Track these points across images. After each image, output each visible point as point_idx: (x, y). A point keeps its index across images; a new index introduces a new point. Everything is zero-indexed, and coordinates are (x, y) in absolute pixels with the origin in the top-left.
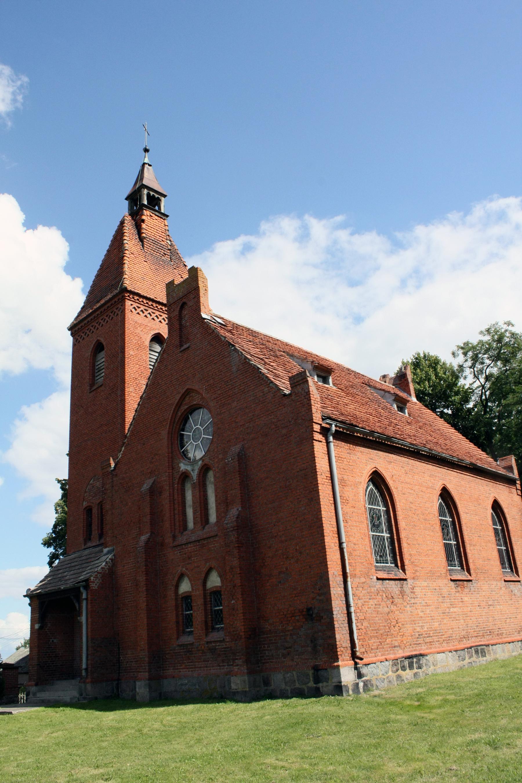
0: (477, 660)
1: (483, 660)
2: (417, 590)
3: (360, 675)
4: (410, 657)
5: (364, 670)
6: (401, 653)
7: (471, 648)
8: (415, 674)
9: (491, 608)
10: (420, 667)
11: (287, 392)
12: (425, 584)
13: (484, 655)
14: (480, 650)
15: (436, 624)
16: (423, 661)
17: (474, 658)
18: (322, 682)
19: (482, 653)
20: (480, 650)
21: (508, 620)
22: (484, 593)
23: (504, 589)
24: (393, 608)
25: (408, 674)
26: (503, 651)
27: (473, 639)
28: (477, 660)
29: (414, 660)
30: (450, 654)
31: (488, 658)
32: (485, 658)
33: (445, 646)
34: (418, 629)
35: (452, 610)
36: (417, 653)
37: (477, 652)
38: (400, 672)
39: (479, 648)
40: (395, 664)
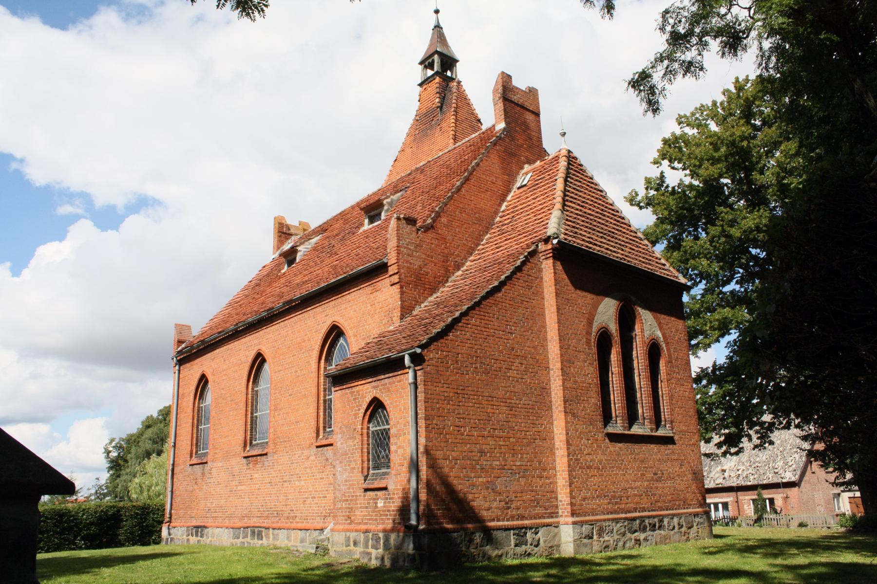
0: (251, 542)
1: (257, 542)
2: (214, 471)
3: (170, 534)
4: (197, 527)
5: (171, 531)
6: (195, 523)
7: (247, 527)
8: (198, 541)
9: (286, 484)
10: (201, 537)
11: (665, 242)
12: (220, 464)
13: (260, 537)
14: (257, 532)
15: (223, 502)
16: (206, 531)
17: (249, 539)
18: (404, 532)
19: (258, 535)
20: (257, 532)
21: (309, 501)
22: (280, 467)
23: (313, 458)
24: (196, 487)
25: (193, 539)
26: (288, 538)
27: (255, 520)
28: (251, 542)
29: (199, 530)
30: (226, 530)
31: (264, 541)
32: (260, 542)
33: (227, 523)
34: (209, 505)
35: (239, 488)
36: (202, 524)
37: (253, 533)
38: (190, 537)
39: (256, 530)
40: (188, 530)
